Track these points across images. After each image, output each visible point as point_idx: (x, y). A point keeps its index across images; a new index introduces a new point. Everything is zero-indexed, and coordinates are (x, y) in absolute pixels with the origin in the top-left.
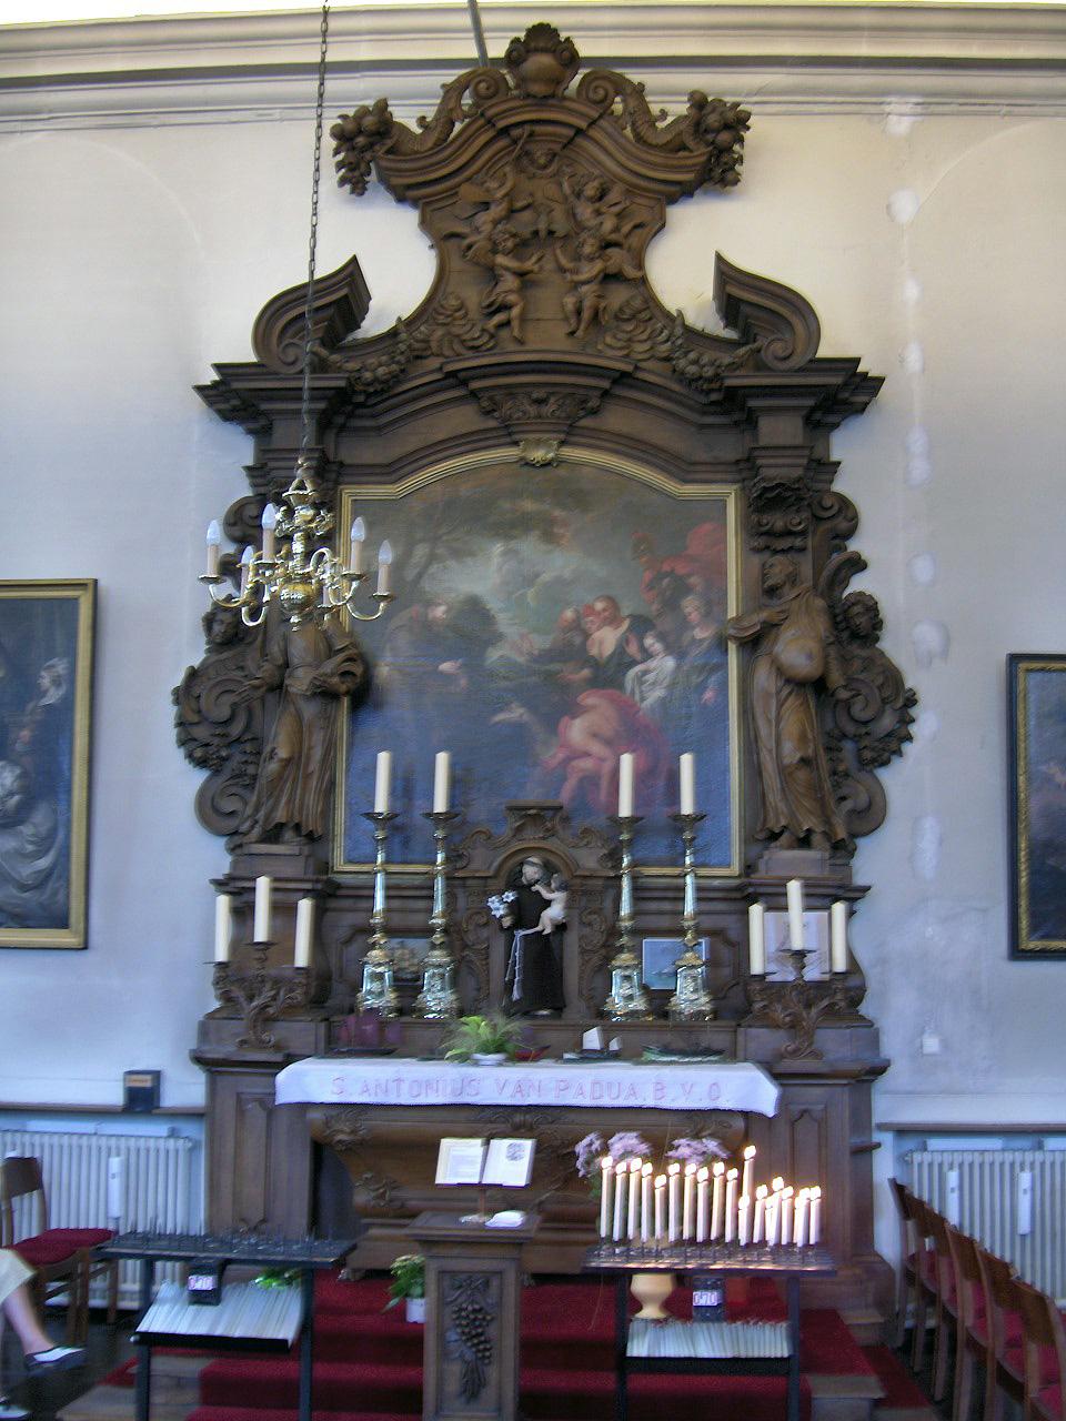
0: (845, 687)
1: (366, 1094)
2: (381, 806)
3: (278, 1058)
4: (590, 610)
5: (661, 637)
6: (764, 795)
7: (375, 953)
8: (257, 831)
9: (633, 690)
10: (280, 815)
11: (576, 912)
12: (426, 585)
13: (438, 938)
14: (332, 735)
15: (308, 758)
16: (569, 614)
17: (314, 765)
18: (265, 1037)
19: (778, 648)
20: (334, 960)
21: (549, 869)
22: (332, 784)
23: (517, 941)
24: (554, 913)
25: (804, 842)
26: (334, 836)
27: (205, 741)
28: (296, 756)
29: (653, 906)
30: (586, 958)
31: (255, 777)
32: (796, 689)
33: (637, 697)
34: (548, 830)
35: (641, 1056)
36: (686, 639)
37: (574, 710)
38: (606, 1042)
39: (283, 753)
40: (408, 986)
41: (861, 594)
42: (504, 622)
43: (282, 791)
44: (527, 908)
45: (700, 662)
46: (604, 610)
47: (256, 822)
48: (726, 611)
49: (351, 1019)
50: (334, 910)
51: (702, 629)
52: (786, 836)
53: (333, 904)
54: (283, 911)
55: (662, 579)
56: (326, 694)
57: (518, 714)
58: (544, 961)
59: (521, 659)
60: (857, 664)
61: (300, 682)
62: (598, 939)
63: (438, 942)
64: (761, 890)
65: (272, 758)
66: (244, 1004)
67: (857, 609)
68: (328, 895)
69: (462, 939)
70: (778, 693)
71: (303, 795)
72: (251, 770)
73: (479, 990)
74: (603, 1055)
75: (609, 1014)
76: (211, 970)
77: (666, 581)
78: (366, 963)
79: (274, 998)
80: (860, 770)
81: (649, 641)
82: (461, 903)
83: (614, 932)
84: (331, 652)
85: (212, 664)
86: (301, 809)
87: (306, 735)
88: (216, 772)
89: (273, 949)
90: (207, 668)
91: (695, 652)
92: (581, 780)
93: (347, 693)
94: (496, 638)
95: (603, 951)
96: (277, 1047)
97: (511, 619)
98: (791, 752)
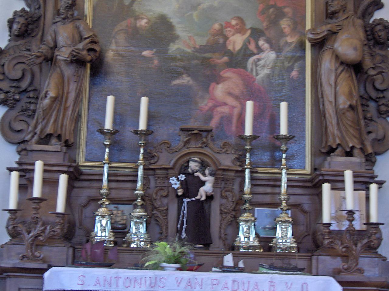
0: (373, 68)
1: (98, 285)
2: (108, 125)
3: (45, 266)
4: (228, 24)
5: (268, 41)
6: (326, 128)
7: (102, 210)
8: (36, 138)
9: (252, 69)
10: (49, 130)
11: (218, 190)
12: (136, 7)
13: (139, 202)
14: (81, 86)
15: (67, 99)
16: (217, 26)
17: (70, 103)
18: (37, 254)
19: (336, 45)
20: (77, 216)
21: (203, 165)
22: (79, 116)
23: (185, 204)
24: (207, 188)
25: (349, 154)
26: (80, 145)
27: (6, 90)
28: (60, 96)
29: (261, 190)
30: (224, 216)
31: (34, 111)
32: (346, 68)
33: (254, 73)
34: (204, 143)
35: (258, 270)
36: (282, 43)
37: (218, 79)
38: (236, 264)
39: (52, 94)
40: (120, 231)
41: (381, 19)
42: (179, 30)
43: (51, 116)
44: (192, 185)
45: (289, 55)
46: (237, 24)
47: (35, 133)
48: (305, 27)
49: (88, 246)
50: (78, 187)
51: (291, 37)
52: (339, 149)
53: (78, 184)
54: (50, 183)
55: (270, 8)
56: (78, 61)
57: (186, 81)
58: (200, 214)
59: (189, 50)
60: (378, 58)
61: (63, 54)
62: (230, 206)
63: (139, 204)
64: (327, 178)
65: (46, 97)
66: (26, 234)
67: (379, 27)
68: (76, 176)
69: (153, 205)
70: (336, 70)
71: (63, 120)
72: (32, 107)
73: (161, 233)
74: (235, 269)
75: (238, 248)
76: (8, 215)
77: (271, 10)
78: (97, 215)
79: (43, 231)
80: (379, 118)
81: (261, 43)
82: (152, 183)
83: (240, 201)
84: (81, 39)
85: (12, 47)
86: (62, 128)
87: (66, 85)
88: (12, 108)
89: (44, 203)
90: (9, 49)
91: (287, 49)
92: (222, 118)
93: (91, 61)
94: (175, 38)
95: (234, 213)
96: (44, 261)
97: (183, 28)
98: (343, 102)
